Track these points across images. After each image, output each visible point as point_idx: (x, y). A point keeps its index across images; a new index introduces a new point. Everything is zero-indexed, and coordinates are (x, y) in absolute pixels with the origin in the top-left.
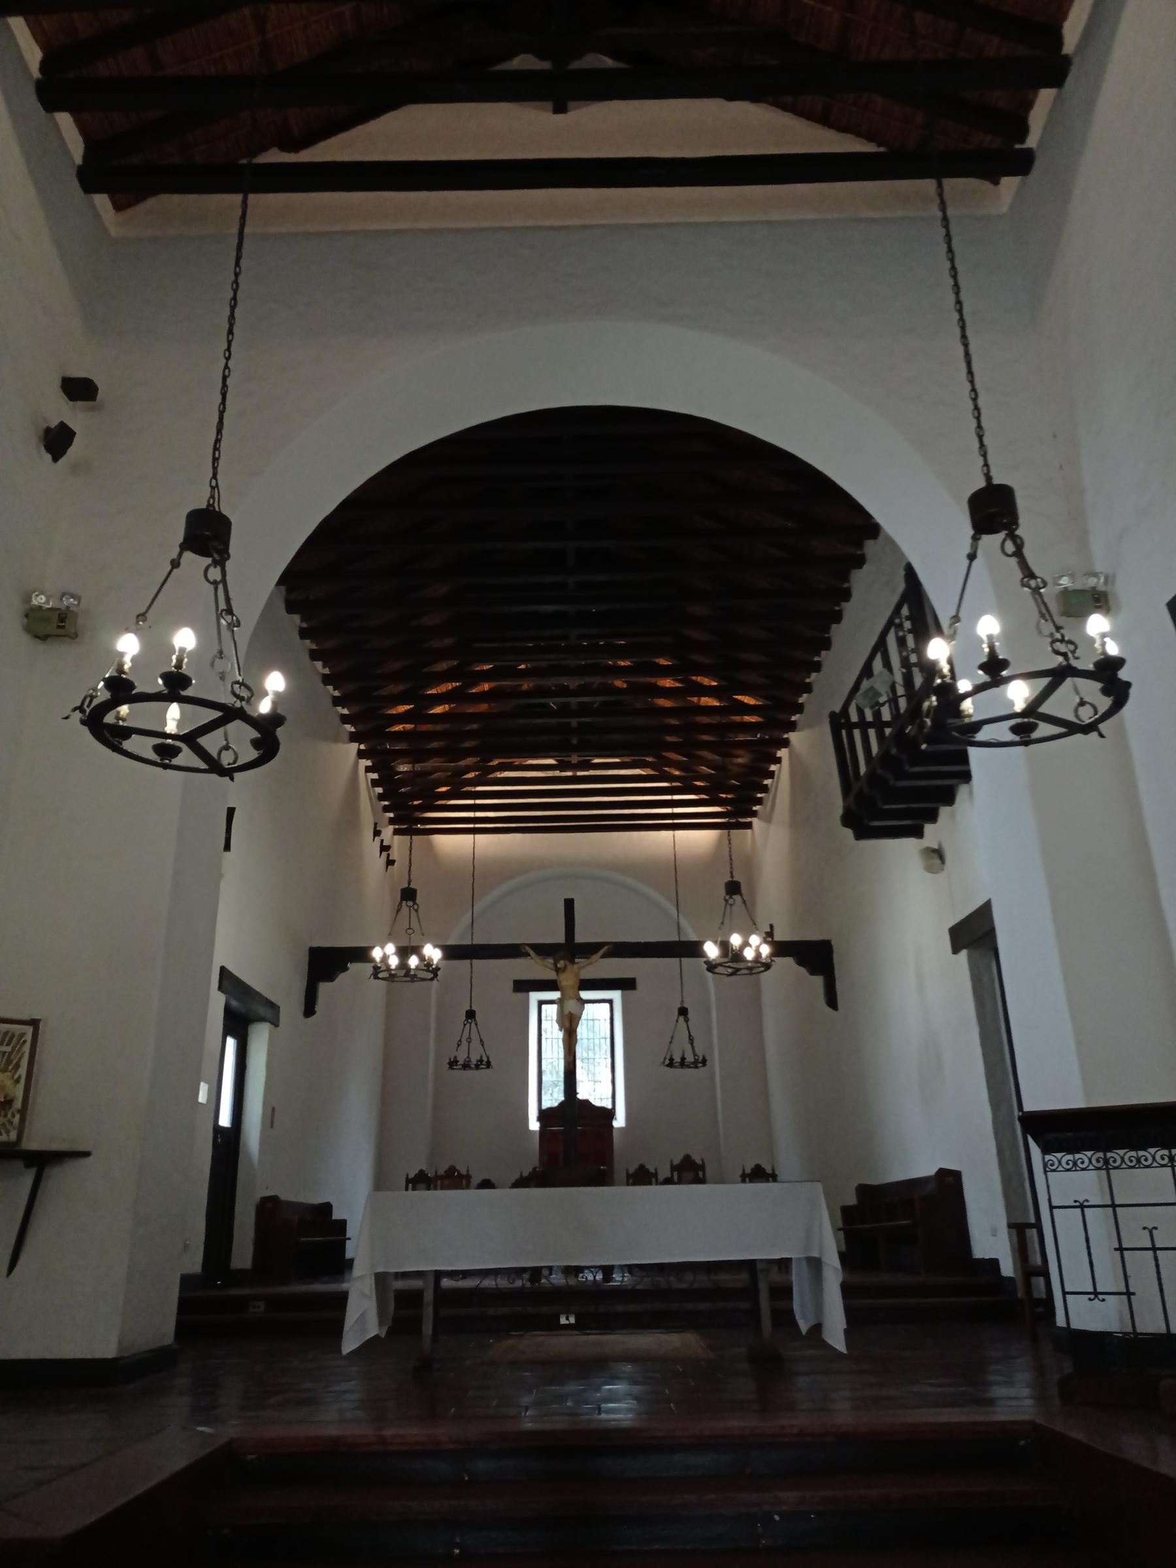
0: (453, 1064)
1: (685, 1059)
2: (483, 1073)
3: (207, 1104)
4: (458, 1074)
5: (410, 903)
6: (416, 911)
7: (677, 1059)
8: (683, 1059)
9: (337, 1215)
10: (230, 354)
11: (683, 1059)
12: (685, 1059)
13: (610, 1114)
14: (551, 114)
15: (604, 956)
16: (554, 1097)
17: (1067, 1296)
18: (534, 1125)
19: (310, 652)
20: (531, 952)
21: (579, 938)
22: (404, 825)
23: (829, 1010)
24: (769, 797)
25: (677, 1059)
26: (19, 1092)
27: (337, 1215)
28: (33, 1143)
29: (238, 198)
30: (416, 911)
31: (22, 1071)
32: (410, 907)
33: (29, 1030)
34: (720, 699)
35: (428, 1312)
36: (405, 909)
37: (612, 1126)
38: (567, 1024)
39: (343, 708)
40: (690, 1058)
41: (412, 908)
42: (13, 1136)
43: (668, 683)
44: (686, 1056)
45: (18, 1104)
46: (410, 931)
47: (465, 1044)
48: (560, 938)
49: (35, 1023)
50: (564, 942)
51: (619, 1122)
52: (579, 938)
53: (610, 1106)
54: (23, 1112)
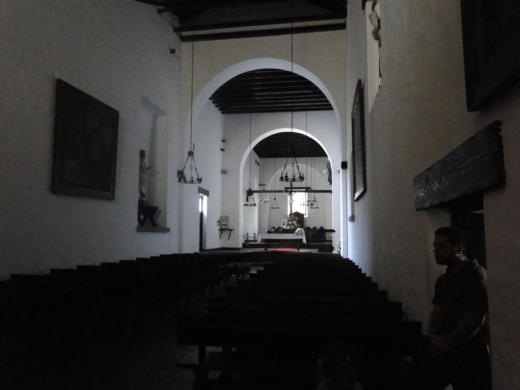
1: (288, 177)
3: (312, 229)
5: (191, 157)
6: (194, 159)
9: (318, 228)
10: (298, 167)
12: (288, 177)
14: (342, 161)
19: (370, 277)
20: (284, 192)
22: (287, 198)
27: (318, 228)
28: (229, 229)
29: (291, 35)
30: (194, 159)
32: (191, 158)
36: (189, 159)
37: (304, 217)
41: (192, 159)
44: (288, 175)
46: (191, 167)
52: (293, 187)
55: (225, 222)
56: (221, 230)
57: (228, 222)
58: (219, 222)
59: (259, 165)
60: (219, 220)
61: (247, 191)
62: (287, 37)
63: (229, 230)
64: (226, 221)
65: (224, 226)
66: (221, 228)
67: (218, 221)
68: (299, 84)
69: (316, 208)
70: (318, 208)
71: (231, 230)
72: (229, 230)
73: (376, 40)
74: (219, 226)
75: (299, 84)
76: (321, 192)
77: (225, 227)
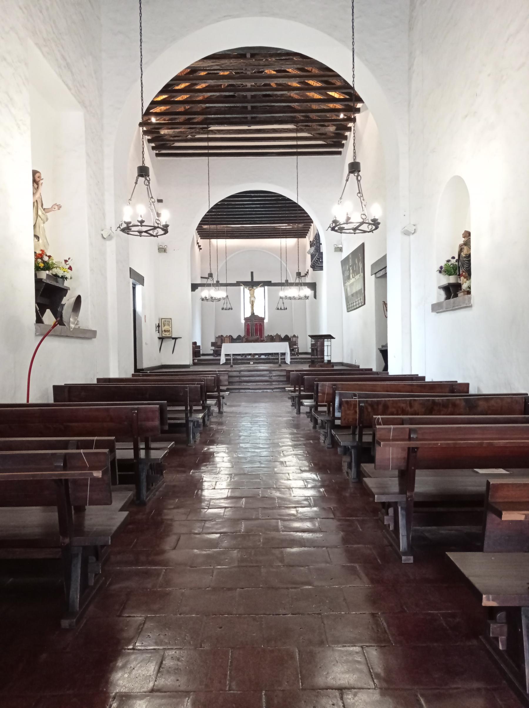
0: (222, 309)
2: (230, 311)
4: (224, 311)
7: (279, 308)
8: (281, 308)
11: (281, 308)
13: (263, 319)
15: (260, 287)
16: (248, 314)
17: (174, 340)
18: (243, 321)
21: (255, 280)
23: (315, 299)
24: (350, 135)
25: (279, 308)
26: (171, 329)
28: (173, 336)
31: (171, 326)
33: (170, 320)
34: (321, 94)
35: (232, 361)
38: (252, 303)
39: (148, 136)
40: (283, 308)
42: (171, 335)
43: (295, 84)
45: (171, 331)
47: (225, 304)
48: (249, 279)
49: (171, 319)
50: (251, 281)
51: (266, 321)
52: (255, 280)
53: (263, 317)
54: (172, 332)
55: (166, 328)
56: (162, 339)
57: (171, 326)
58: (159, 326)
59: (201, 249)
60: (159, 324)
61: (271, 281)
62: (205, 158)
63: (173, 338)
64: (169, 325)
65: (165, 333)
66: (161, 336)
67: (157, 325)
68: (292, 207)
69: (225, 309)
70: (232, 309)
71: (176, 339)
72: (173, 338)
73: (404, 454)
74: (159, 332)
75: (292, 207)
76: (303, 353)
77: (167, 334)
